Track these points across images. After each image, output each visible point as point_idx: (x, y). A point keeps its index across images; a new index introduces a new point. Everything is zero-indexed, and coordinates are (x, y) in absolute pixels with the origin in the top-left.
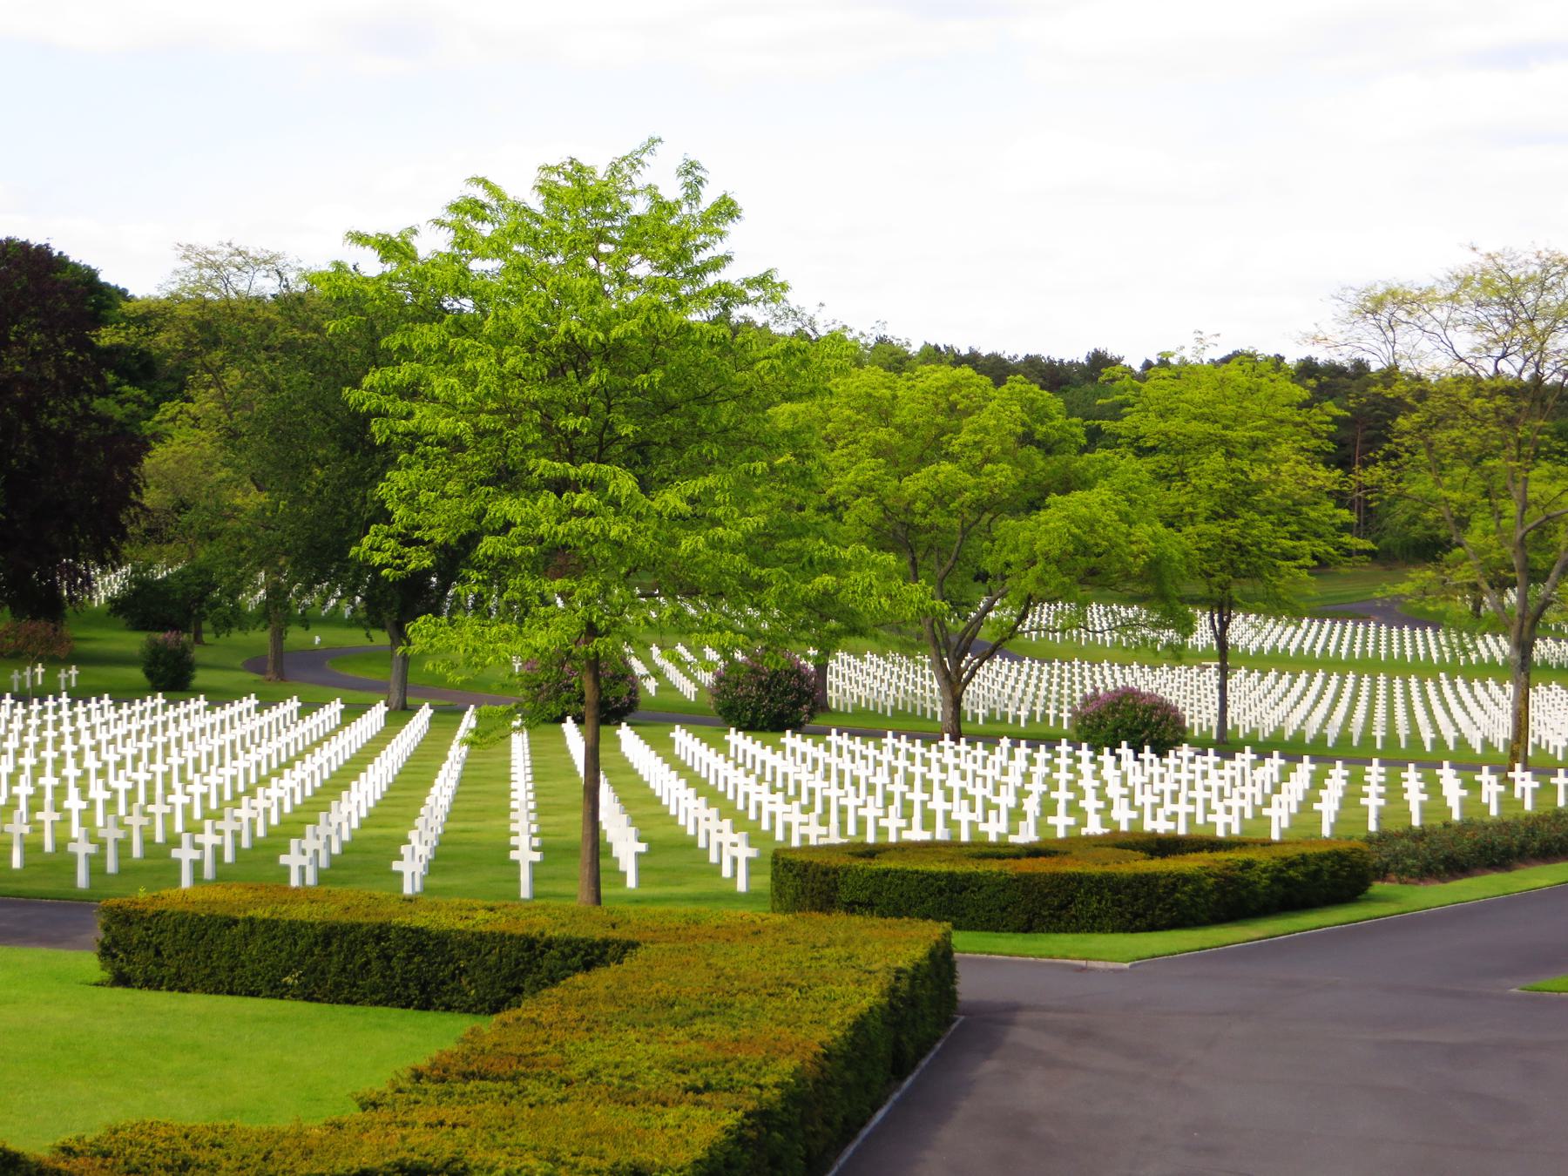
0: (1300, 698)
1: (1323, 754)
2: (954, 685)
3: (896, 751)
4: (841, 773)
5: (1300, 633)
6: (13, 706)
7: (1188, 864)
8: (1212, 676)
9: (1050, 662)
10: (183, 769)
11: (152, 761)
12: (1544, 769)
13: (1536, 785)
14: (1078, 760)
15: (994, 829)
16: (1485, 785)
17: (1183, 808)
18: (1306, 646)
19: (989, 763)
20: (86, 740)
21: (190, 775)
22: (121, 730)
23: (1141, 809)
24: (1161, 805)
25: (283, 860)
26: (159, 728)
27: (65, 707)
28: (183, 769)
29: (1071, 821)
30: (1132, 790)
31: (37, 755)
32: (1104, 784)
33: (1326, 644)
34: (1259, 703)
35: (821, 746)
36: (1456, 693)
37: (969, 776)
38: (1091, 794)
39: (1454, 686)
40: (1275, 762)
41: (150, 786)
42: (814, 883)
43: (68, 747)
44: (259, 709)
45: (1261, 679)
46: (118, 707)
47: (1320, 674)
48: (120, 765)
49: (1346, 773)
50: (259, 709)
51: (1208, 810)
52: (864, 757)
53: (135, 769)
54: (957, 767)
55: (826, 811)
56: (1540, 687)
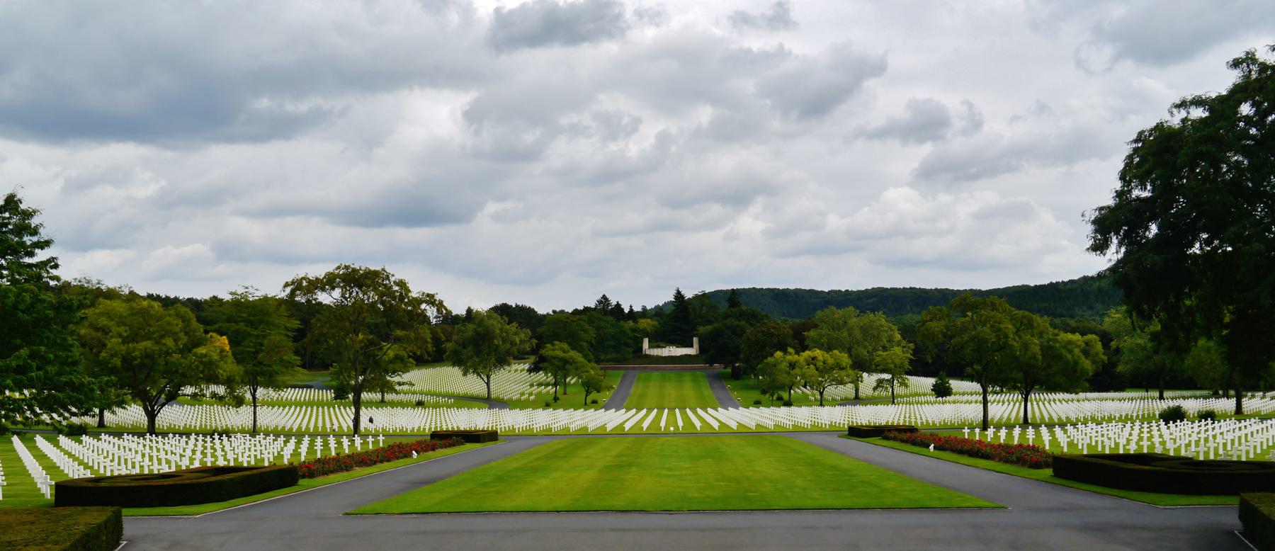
1: (288, 435)
2: (152, 416)
12: (364, 436)
15: (185, 464)
17: (253, 453)
34: (268, 417)
42: (69, 493)
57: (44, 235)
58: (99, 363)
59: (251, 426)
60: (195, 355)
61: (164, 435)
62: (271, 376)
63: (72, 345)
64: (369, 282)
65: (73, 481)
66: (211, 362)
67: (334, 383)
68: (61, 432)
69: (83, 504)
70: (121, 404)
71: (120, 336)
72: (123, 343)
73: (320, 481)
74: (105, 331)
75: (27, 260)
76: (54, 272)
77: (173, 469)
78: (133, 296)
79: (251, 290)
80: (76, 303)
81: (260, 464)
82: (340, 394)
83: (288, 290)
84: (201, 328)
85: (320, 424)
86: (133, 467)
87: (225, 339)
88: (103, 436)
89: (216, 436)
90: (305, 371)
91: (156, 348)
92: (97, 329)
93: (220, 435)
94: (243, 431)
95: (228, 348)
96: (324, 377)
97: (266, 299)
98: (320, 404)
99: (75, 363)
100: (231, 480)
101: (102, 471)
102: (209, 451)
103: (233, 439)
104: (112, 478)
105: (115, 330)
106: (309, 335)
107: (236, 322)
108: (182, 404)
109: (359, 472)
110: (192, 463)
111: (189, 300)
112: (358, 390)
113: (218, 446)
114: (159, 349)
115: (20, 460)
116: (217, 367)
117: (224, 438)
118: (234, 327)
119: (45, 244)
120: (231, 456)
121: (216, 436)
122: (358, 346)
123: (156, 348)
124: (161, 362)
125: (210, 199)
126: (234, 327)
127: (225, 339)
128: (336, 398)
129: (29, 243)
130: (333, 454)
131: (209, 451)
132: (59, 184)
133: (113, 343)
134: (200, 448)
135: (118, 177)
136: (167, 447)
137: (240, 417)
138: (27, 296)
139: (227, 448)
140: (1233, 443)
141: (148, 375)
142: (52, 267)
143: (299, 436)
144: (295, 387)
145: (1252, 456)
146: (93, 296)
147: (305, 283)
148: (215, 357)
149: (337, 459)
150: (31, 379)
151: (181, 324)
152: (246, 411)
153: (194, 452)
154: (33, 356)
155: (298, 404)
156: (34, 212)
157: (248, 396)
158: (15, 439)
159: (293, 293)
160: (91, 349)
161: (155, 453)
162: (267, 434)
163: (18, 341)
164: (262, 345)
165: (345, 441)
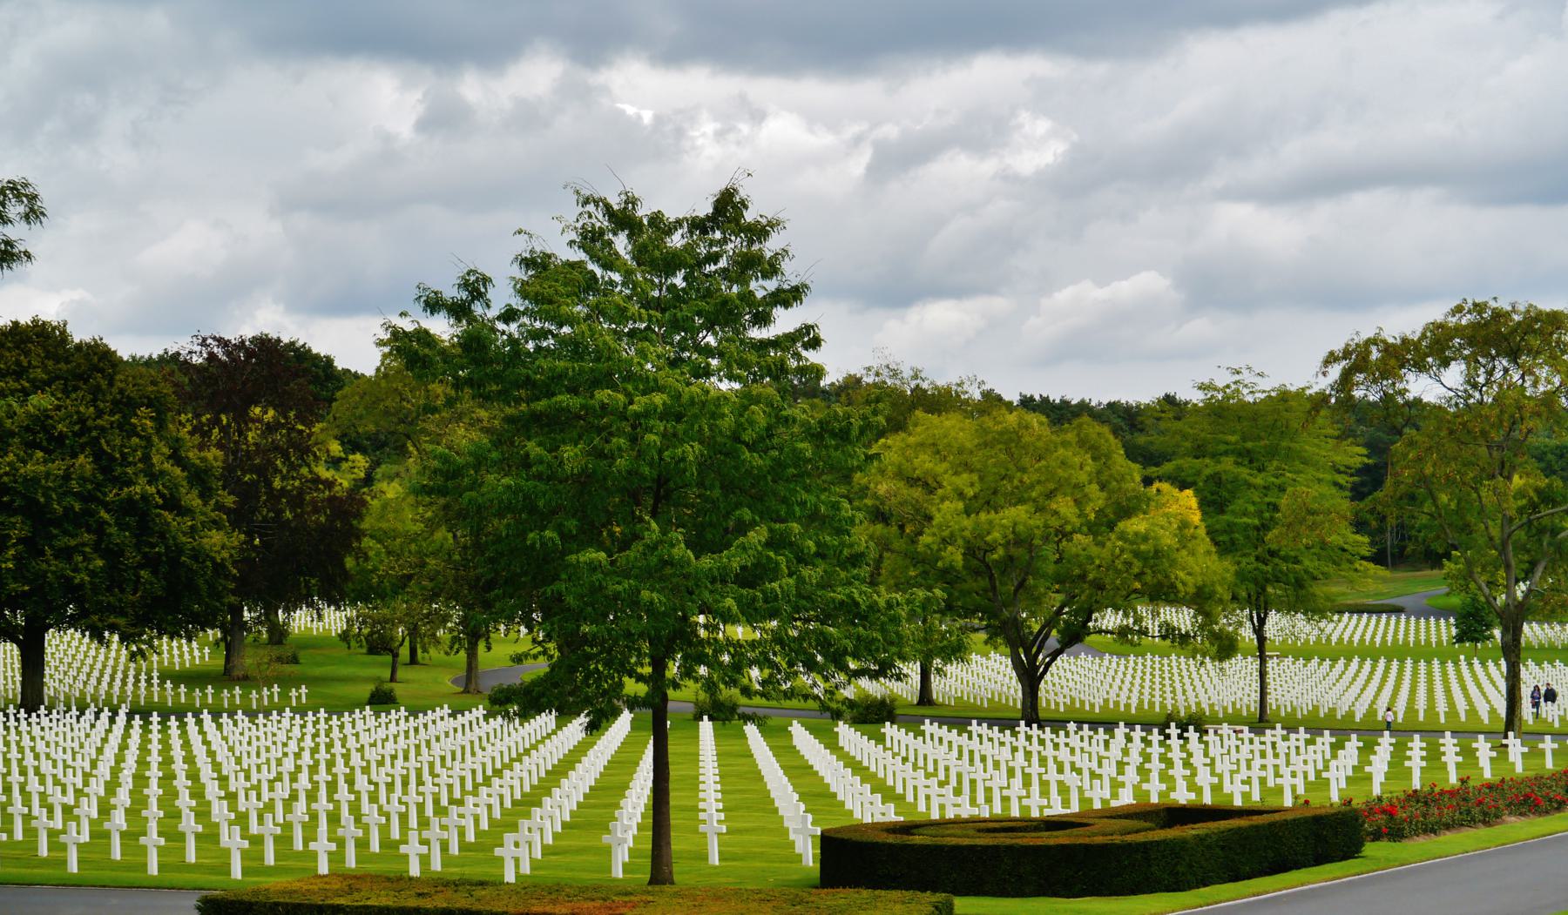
0: (1354, 679)
1: (1341, 729)
2: (1030, 678)
3: (1029, 738)
4: (971, 752)
5: (1342, 625)
6: (292, 719)
7: (1257, 820)
8: (1253, 665)
9: (1143, 656)
10: (431, 765)
11: (418, 754)
13: (1556, 746)
14: (1168, 737)
15: (1099, 795)
16: (1510, 749)
17: (1256, 773)
18: (1368, 638)
19: (1094, 741)
20: (352, 743)
21: (438, 769)
22: (382, 733)
23: (1220, 776)
24: (1237, 771)
25: (498, 851)
26: (412, 733)
27: (322, 721)
28: (431, 765)
29: (1164, 787)
30: (1213, 760)
31: (312, 757)
32: (1190, 755)
33: (1363, 635)
34: (1294, 686)
35: (965, 735)
36: (1488, 675)
37: (1078, 751)
38: (1178, 764)
39: (1470, 665)
40: (1328, 738)
41: (419, 772)
42: (851, 858)
43: (338, 749)
44: (453, 715)
45: (1332, 667)
46: (377, 715)
47: (1382, 661)
48: (381, 763)
49: (1393, 741)
50: (486, 718)
51: (1277, 775)
52: (990, 740)
53: (405, 792)
54: (1067, 745)
55: (959, 782)
56: (1530, 662)
57: (791, 273)
58: (916, 559)
59: (1254, 707)
60: (1122, 536)
61: (1058, 724)
62: (1299, 584)
63: (852, 521)
64: (1536, 342)
65: (862, 828)
66: (1158, 553)
67: (1455, 601)
68: (837, 715)
69: (875, 885)
70: (956, 651)
71: (961, 495)
72: (968, 512)
73: (1417, 847)
74: (929, 485)
75: (756, 333)
76: (812, 357)
77: (1075, 808)
78: (992, 400)
79: (1247, 377)
80: (856, 423)
81: (1271, 802)
82: (1471, 627)
83: (1335, 371)
84: (1136, 471)
85: (1421, 704)
86: (989, 800)
87: (1189, 498)
88: (928, 727)
89: (1173, 731)
90: (1381, 571)
91: (1038, 521)
92: (912, 481)
93: (1183, 728)
94: (1234, 719)
95: (1196, 517)
96: (1431, 585)
97: (1284, 396)
98: (1422, 653)
99: (856, 560)
100: (1200, 839)
101: (922, 807)
102: (1156, 765)
103: (1210, 737)
104: (943, 823)
105: (950, 482)
106: (1389, 481)
107: (1214, 456)
108: (1098, 652)
109: (1518, 828)
110: (1115, 795)
111: (1112, 406)
112: (1513, 620)
113: (1176, 755)
114: (1037, 530)
115: (758, 777)
116: (1173, 563)
117: (1192, 734)
118: (1208, 467)
119: (790, 296)
120: (1204, 778)
121: (1173, 731)
122: (1512, 506)
123: (1038, 521)
124: (1049, 552)
125: (1178, 165)
126: (1208, 467)
127: (1189, 498)
128: (1460, 639)
129: (760, 294)
130: (1453, 780)
131: (1156, 765)
132: (858, 165)
133: (946, 511)
134: (1135, 758)
135: (981, 131)
136: (1064, 754)
137: (1230, 685)
138: (759, 414)
139: (1198, 760)
140: (390, 786)
141: (1021, 585)
142: (806, 346)
143: (1370, 731)
144: (1358, 610)
145: (436, 865)
146: (895, 406)
147: (1375, 354)
148: (1168, 540)
149: (1460, 794)
150: (770, 598)
151: (1091, 465)
152: (1242, 668)
153: (1121, 766)
154: (775, 543)
155: (1368, 652)
156: (770, 224)
157: (1247, 634)
158: (751, 730)
159: (1346, 380)
160: (902, 527)
161: (1035, 769)
162: (1291, 728)
163: (746, 514)
164: (1276, 508)
165: (1483, 748)
